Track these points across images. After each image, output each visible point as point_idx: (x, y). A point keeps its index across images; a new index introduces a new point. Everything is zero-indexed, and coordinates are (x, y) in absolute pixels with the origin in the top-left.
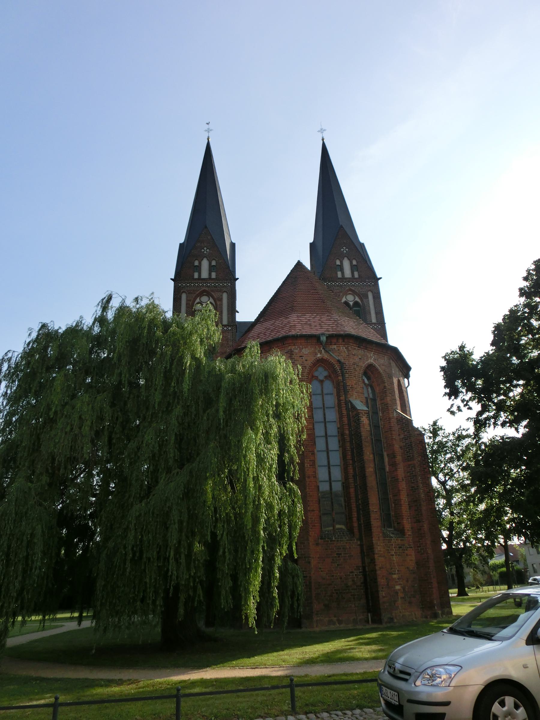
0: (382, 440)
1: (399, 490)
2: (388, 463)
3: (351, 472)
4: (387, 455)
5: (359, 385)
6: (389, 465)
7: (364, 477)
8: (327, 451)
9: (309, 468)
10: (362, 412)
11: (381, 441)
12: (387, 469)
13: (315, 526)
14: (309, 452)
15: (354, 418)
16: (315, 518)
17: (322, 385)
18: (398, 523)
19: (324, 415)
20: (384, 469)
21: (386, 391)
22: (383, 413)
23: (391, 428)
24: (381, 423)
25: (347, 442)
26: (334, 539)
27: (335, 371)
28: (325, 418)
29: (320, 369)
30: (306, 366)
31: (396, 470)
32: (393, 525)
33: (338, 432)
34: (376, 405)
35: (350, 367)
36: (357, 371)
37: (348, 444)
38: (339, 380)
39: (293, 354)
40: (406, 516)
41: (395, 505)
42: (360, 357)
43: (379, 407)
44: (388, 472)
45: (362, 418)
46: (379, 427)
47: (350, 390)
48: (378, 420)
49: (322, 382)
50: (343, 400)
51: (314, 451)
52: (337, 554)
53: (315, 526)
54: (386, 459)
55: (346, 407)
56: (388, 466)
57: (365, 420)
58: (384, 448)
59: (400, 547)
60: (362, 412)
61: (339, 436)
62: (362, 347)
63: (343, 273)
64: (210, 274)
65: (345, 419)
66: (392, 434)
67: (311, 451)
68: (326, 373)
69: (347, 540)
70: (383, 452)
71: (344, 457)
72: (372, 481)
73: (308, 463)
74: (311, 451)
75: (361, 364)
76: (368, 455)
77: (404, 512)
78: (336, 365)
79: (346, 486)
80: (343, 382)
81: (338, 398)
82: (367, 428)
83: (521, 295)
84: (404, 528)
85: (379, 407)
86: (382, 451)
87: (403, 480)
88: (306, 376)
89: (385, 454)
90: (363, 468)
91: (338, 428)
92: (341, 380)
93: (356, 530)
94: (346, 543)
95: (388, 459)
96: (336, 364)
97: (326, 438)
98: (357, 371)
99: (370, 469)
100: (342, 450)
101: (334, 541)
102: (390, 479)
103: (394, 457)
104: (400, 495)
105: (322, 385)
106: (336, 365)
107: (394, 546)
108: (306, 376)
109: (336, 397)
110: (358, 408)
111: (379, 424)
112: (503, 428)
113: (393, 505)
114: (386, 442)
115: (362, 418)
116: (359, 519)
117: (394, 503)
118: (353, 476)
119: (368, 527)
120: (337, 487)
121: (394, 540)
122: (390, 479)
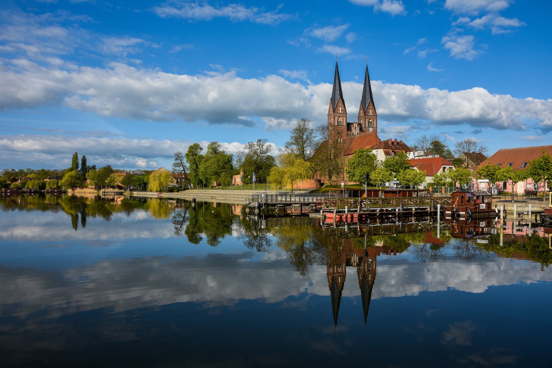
63: (370, 114)
64: (341, 112)
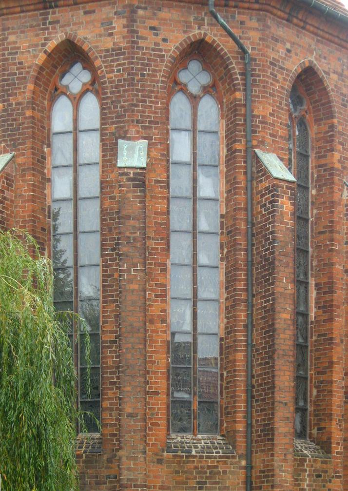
0: (310, 250)
1: (331, 362)
2: (316, 303)
3: (243, 318)
4: (316, 285)
5: (279, 117)
6: (318, 307)
7: (270, 331)
8: (195, 267)
9: (155, 301)
10: (281, 184)
11: (307, 252)
12: (312, 315)
13: (158, 425)
14: (155, 264)
15: (263, 196)
16: (159, 409)
17: (195, 109)
18: (319, 429)
19: (195, 181)
20: (305, 315)
21: (332, 136)
22: (319, 188)
23: (332, 226)
24: (312, 213)
25: (240, 249)
26: (194, 453)
27: (228, 76)
28: (195, 189)
29: (194, 66)
30: (163, 56)
31: (331, 320)
32: (308, 432)
33: (222, 223)
34: (307, 168)
35: (264, 71)
36: (278, 81)
37: (242, 255)
38: (235, 99)
39: (136, 22)
40: (337, 416)
41: (318, 392)
42: (288, 46)
43: (312, 173)
44: (312, 322)
45: (280, 200)
46: (307, 220)
47: (258, 126)
48: (308, 205)
49: (194, 100)
50: (240, 151)
51: (165, 264)
52: (198, 483)
53: (158, 425)
54: (313, 294)
55: (246, 167)
56: (314, 310)
57: (285, 205)
58: (312, 270)
59: (319, 476)
60: (281, 184)
61: (222, 233)
62: (295, 20)
65: (241, 197)
66: (332, 240)
67: (159, 264)
68: (205, 79)
69: (220, 457)
70: (307, 278)
71: (230, 282)
72: (285, 339)
73: (151, 290)
74: (159, 264)
75: (287, 65)
76: (284, 284)
77: (334, 408)
78: (234, 62)
79: (227, 347)
80: (245, 105)
81: (227, 145)
82: (287, 224)
83: (124, 27)
84: (329, 438)
85: (312, 173)
86: (306, 274)
87: (342, 341)
88: (162, 82)
89: (312, 282)
90: (270, 312)
91: (222, 216)
92: (240, 100)
93: (241, 440)
94: (218, 462)
95: (317, 294)
96: (234, 58)
97: (194, 237)
98: (278, 81)
99: (284, 315)
100: (227, 268)
101: (195, 456)
102: (314, 338)
103: (331, 291)
104: (331, 371)
105: (195, 109)
106: (234, 62)
107: (308, 473)
108: (162, 82)
109: (225, 141)
110: (275, 175)
111: (307, 213)
112: (220, 260)
113: (315, 392)
114: (317, 256)
115: (280, 200)
116: (248, 415)
117: (316, 387)
118: (246, 326)
119: (268, 433)
120: (208, 349)
121: (310, 461)
122: (314, 338)
